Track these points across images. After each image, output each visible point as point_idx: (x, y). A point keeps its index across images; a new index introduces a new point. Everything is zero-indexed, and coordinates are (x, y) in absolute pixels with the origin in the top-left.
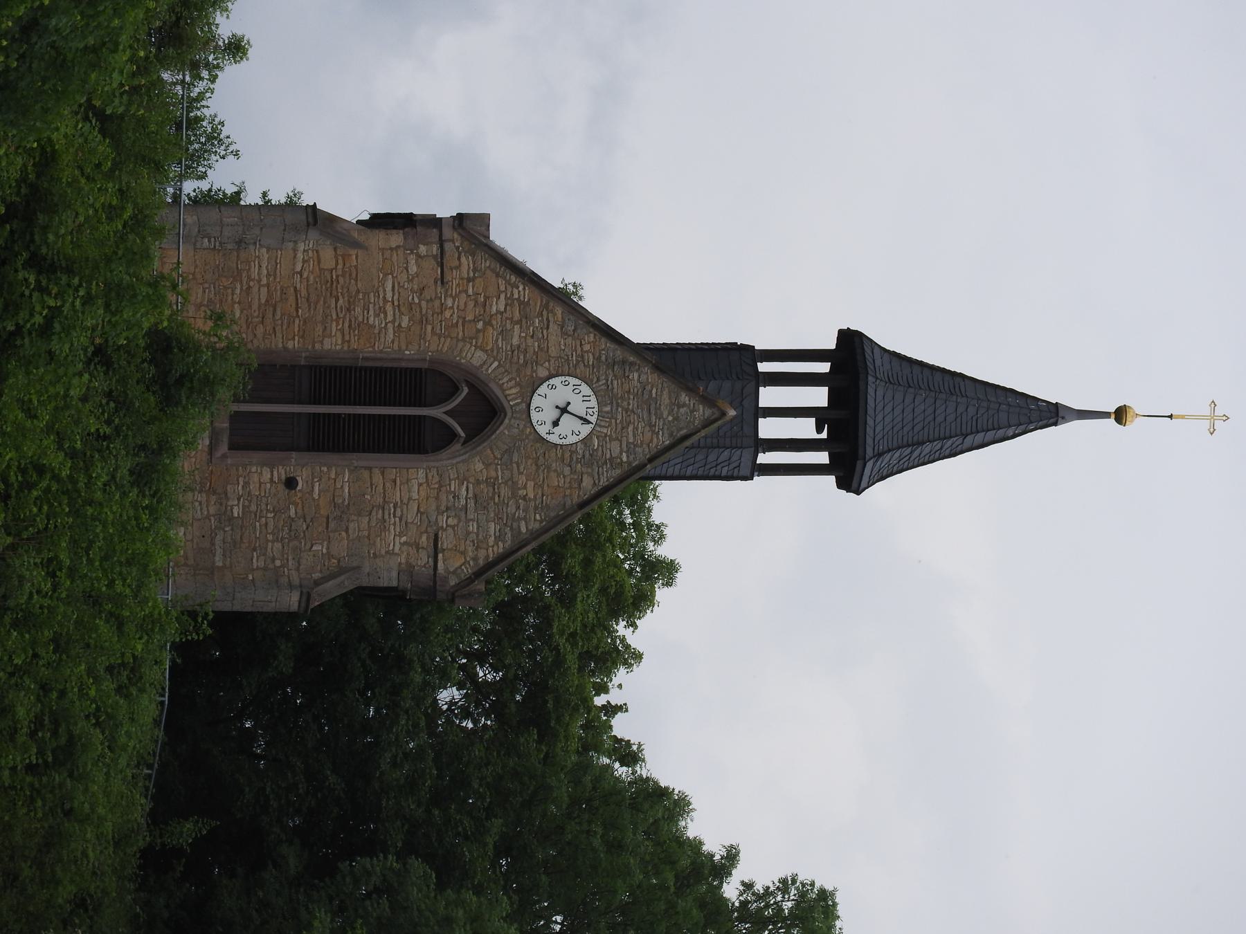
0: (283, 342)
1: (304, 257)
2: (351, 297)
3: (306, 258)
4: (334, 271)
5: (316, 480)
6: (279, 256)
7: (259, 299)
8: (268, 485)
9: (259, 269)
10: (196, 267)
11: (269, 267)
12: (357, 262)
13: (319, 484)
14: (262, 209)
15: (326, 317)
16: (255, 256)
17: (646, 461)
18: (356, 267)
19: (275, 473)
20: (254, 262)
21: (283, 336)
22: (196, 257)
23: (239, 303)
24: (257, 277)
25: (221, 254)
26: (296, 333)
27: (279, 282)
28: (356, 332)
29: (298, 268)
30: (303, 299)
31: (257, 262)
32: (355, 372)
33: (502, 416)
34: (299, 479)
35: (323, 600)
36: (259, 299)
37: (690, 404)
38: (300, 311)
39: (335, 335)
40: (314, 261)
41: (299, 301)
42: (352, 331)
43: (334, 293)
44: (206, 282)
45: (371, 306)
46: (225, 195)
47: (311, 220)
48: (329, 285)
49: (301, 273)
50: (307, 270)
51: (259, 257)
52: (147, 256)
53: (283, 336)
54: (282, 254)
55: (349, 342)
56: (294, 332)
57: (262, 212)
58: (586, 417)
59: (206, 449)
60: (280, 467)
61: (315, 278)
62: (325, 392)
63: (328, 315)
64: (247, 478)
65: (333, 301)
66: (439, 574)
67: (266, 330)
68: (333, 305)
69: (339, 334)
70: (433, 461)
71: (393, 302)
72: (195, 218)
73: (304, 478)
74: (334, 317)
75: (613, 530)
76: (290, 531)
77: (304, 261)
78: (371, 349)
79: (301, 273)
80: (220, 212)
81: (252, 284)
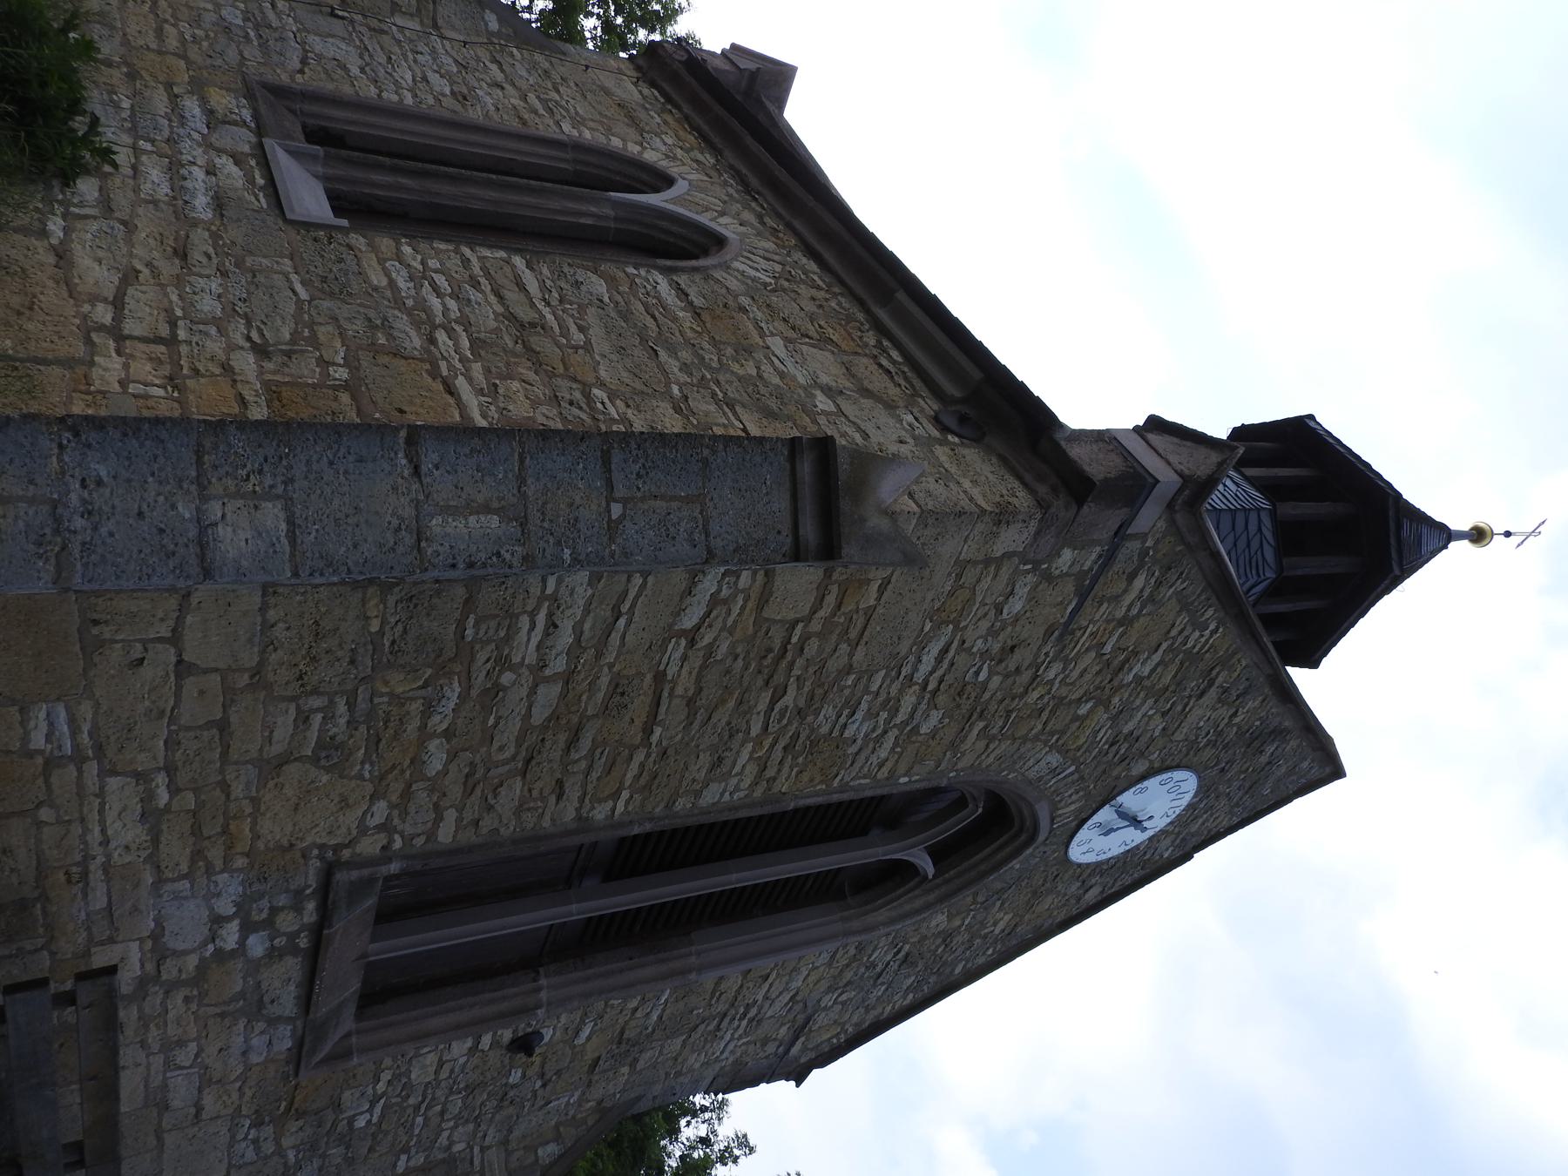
1: (719, 590)
2: (821, 685)
3: (725, 592)
4: (800, 625)
6: (631, 596)
9: (547, 634)
10: (269, 645)
11: (587, 626)
12: (879, 599)
14: (617, 457)
15: (731, 736)
16: (543, 597)
18: (869, 613)
20: (533, 615)
21: (585, 794)
22: (272, 614)
23: (448, 734)
24: (531, 658)
25: (391, 600)
26: (627, 784)
27: (611, 666)
28: (800, 760)
29: (688, 622)
30: (676, 701)
31: (541, 618)
33: (1023, 837)
37: (392, 284)
38: (658, 731)
40: (746, 600)
41: (663, 709)
42: (471, 620)
43: (779, 678)
44: (315, 692)
47: (810, 531)
48: (768, 661)
49: (692, 637)
50: (718, 625)
51: (554, 598)
52: (242, 883)
53: (585, 794)
54: (644, 585)
57: (617, 477)
58: (1150, 833)
61: (733, 646)
65: (766, 696)
68: (762, 706)
71: (924, 687)
72: (272, 515)
74: (755, 730)
75: (71, 296)
76: (225, 831)
77: (715, 601)
79: (692, 637)
80: (416, 471)
81: (507, 678)
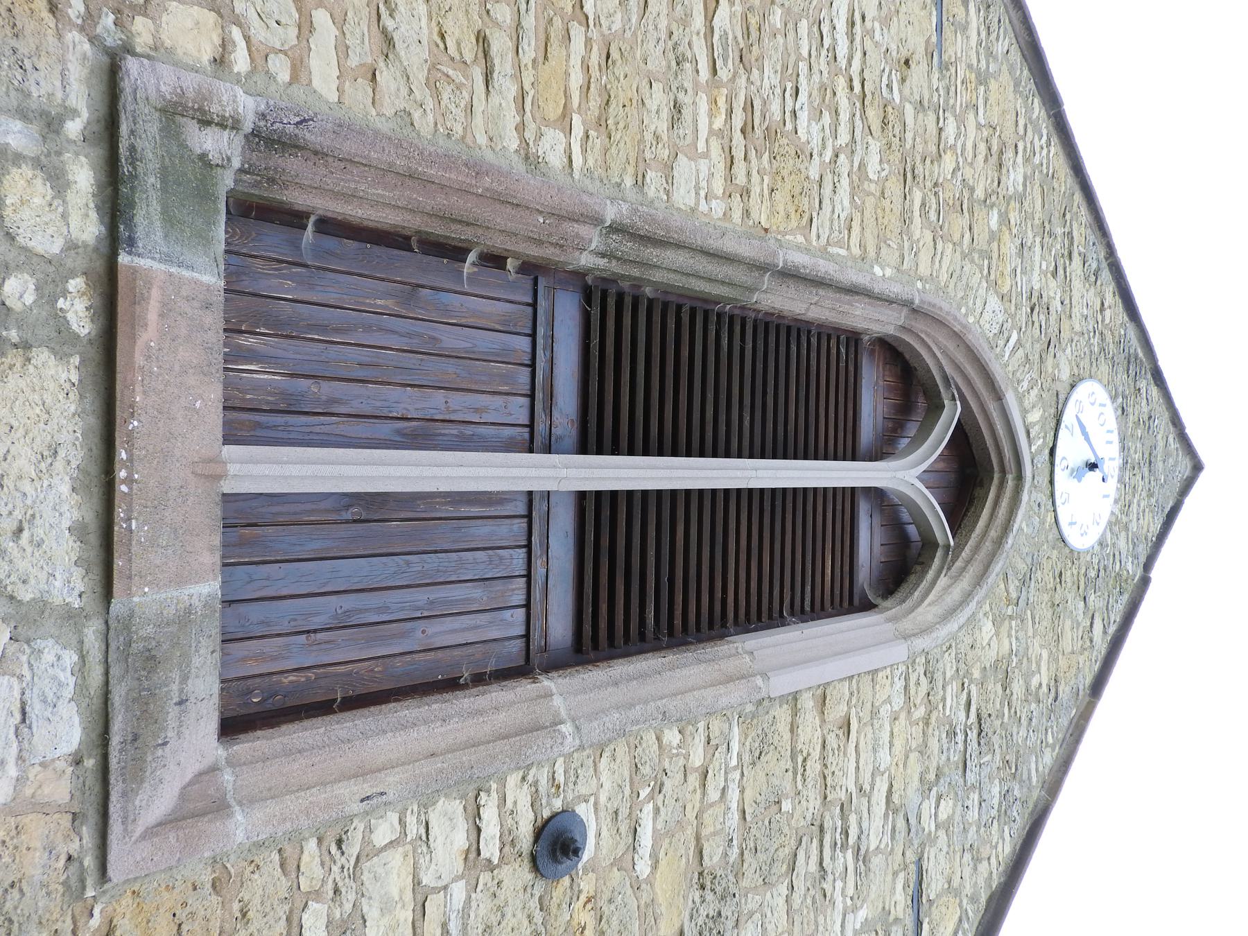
0: (521, 128)
5: (643, 794)
7: (899, 21)
8: (459, 891)
13: (657, 811)
17: (213, 125)
19: (490, 815)
32: (719, 323)
34: (583, 811)
35: (417, 710)
36: (899, 21)
39: (706, 155)
45: (803, 66)
46: (446, 796)
55: (745, 193)
56: (567, 95)
59: (60, 790)
60: (513, 780)
62: (771, 602)
63: (685, 59)
64: (349, 897)
66: (204, 239)
67: (33, 535)
69: (715, 146)
70: (253, 194)
73: (603, 799)
78: (800, 239)
